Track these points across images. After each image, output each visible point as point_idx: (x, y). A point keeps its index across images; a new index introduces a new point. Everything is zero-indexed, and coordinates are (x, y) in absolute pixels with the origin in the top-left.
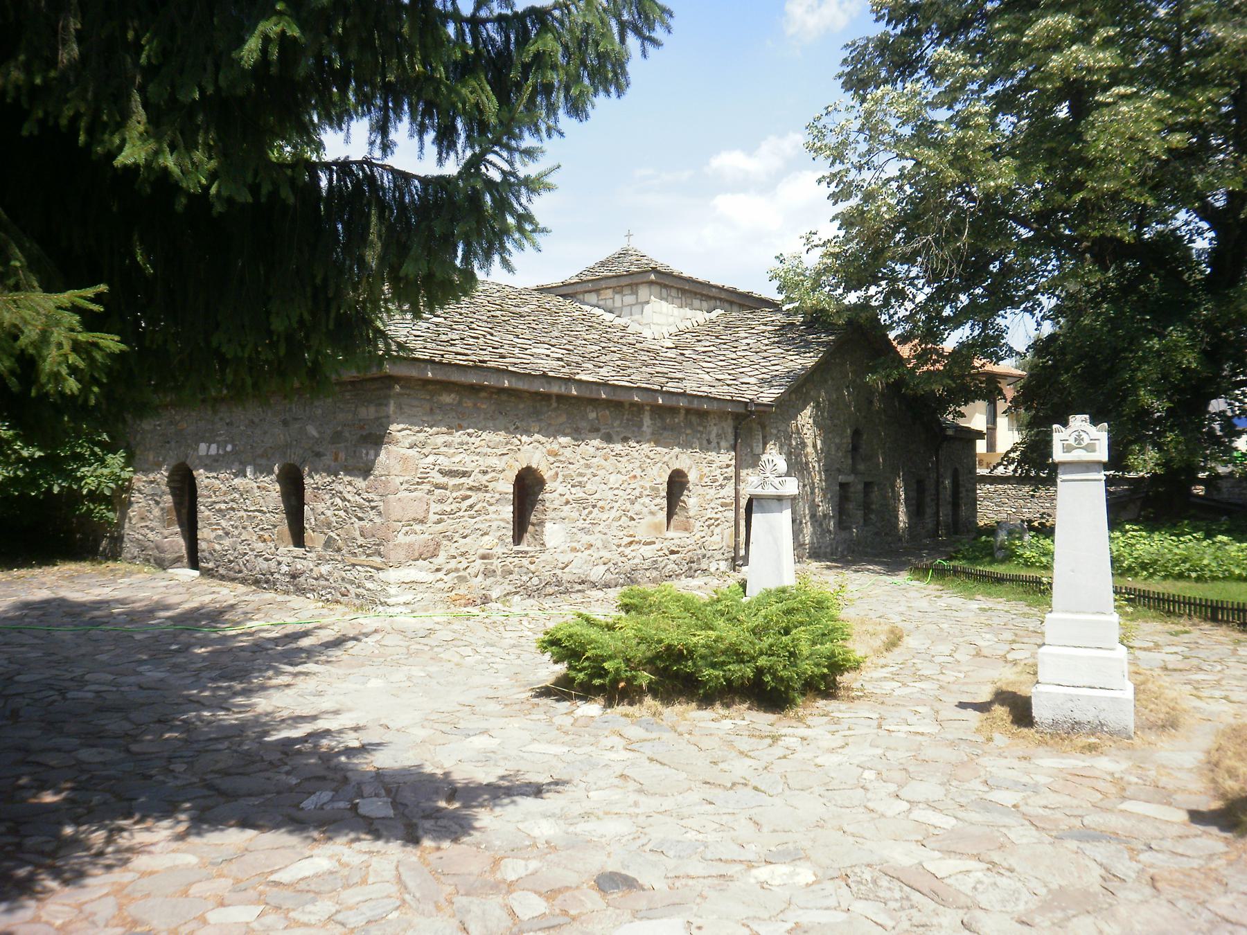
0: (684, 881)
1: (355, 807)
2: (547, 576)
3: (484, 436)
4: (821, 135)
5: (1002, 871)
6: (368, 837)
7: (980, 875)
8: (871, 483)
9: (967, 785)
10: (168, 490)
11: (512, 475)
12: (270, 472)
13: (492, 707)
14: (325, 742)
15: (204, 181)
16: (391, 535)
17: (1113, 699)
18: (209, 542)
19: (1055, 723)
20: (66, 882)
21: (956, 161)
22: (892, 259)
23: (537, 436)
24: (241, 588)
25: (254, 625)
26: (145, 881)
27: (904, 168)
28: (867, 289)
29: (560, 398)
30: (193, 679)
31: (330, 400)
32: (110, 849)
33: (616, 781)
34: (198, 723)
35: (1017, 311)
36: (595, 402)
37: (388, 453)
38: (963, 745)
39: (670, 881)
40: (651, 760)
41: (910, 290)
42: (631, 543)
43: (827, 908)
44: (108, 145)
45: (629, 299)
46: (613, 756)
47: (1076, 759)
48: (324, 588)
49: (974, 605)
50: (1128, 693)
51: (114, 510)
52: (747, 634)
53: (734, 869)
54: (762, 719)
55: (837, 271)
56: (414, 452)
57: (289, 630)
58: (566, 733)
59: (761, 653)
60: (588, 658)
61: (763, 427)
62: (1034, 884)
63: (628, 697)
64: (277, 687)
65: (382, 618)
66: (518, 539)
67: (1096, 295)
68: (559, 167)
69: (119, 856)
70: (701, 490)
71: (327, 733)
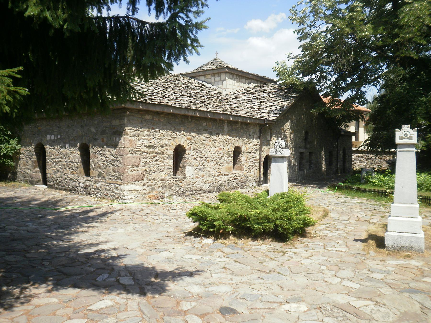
0: (255, 310)
1: (118, 281)
2: (186, 188)
3: (162, 132)
4: (295, 14)
5: (381, 305)
6: (125, 293)
7: (372, 306)
8: (312, 152)
9: (362, 272)
10: (34, 153)
11: (173, 148)
12: (76, 146)
13: (169, 240)
14: (103, 254)
15: (61, 23)
16: (125, 171)
17: (417, 238)
18: (51, 174)
19: (394, 247)
20: (6, 309)
21: (349, 25)
22: (323, 64)
23: (183, 132)
24: (64, 193)
25: (70, 207)
26: (38, 309)
27: (328, 27)
28: (311, 76)
29: (192, 117)
30: (48, 228)
31: (100, 117)
32: (22, 296)
33: (222, 270)
34: (52, 246)
35: (370, 85)
36: (206, 119)
37: (124, 138)
38: (358, 256)
39: (249, 310)
40: (235, 261)
41: (329, 77)
42: (219, 175)
43: (314, 321)
44: (21, 8)
45: (217, 79)
46: (219, 259)
47: (403, 261)
48: (98, 192)
49: (354, 201)
50: (422, 235)
51: (13, 162)
52: (271, 211)
53: (275, 306)
54: (278, 245)
55: (300, 68)
56: (135, 138)
57: (85, 209)
58: (200, 250)
59: (277, 219)
60: (208, 220)
61: (271, 130)
62: (394, 310)
63: (223, 236)
64: (82, 232)
65: (122, 205)
66: (175, 173)
67: (401, 79)
68: (210, 19)
69: (26, 299)
70: (246, 154)
71: (103, 250)
